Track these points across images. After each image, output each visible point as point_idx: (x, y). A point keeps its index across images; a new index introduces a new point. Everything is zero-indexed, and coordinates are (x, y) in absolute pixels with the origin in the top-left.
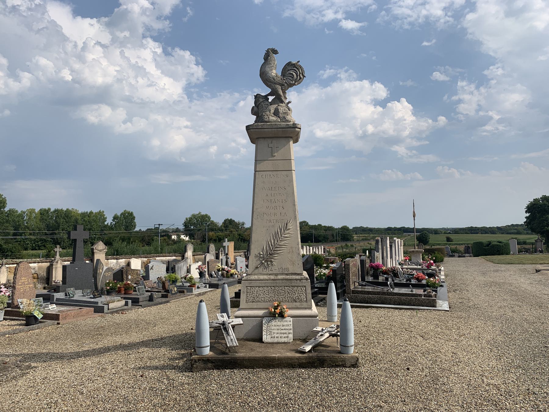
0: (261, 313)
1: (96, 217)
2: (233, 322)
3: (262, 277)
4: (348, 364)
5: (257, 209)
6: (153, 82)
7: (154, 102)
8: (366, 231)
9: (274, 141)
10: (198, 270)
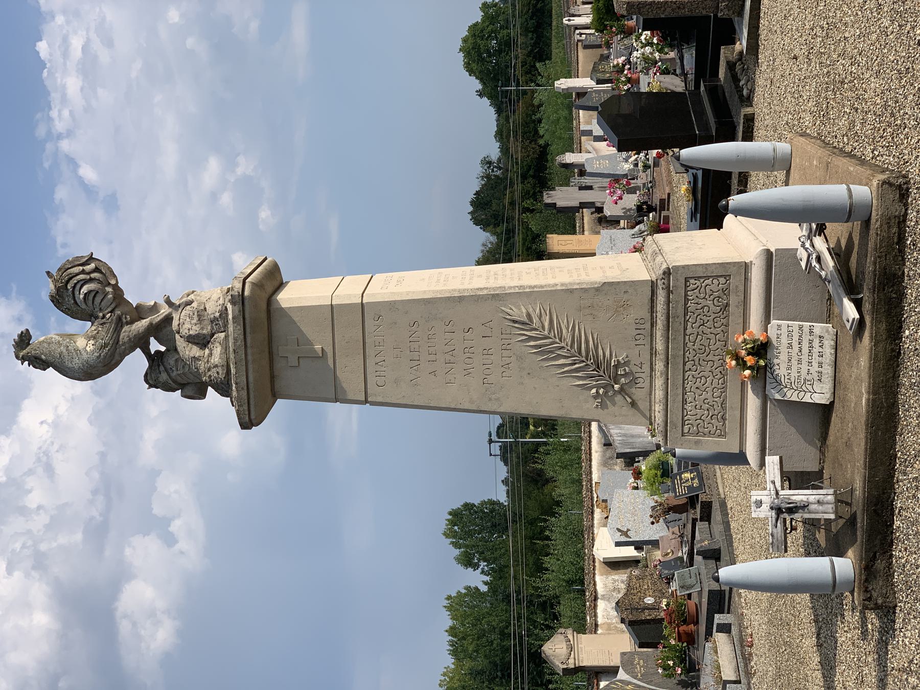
0: (753, 402)
1: (465, 616)
2: (773, 482)
3: (659, 394)
4: (898, 209)
5: (471, 402)
6: (39, 460)
7: (103, 455)
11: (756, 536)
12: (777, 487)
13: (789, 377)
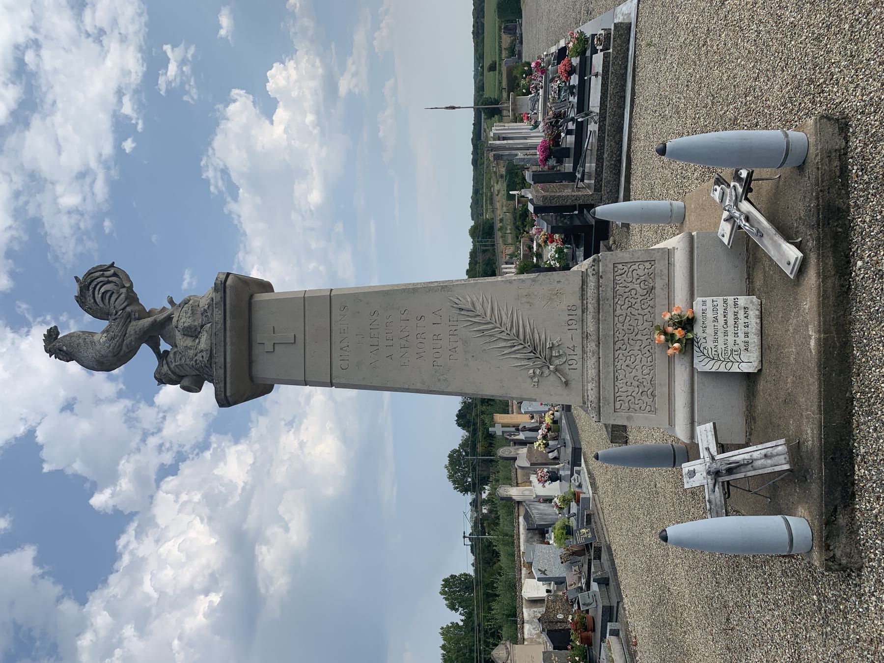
2: (708, 449)
3: (592, 373)
4: (840, 143)
8: (477, 200)
9: (258, 337)
10: (547, 484)
11: (638, 563)
12: (712, 453)
13: (716, 349)
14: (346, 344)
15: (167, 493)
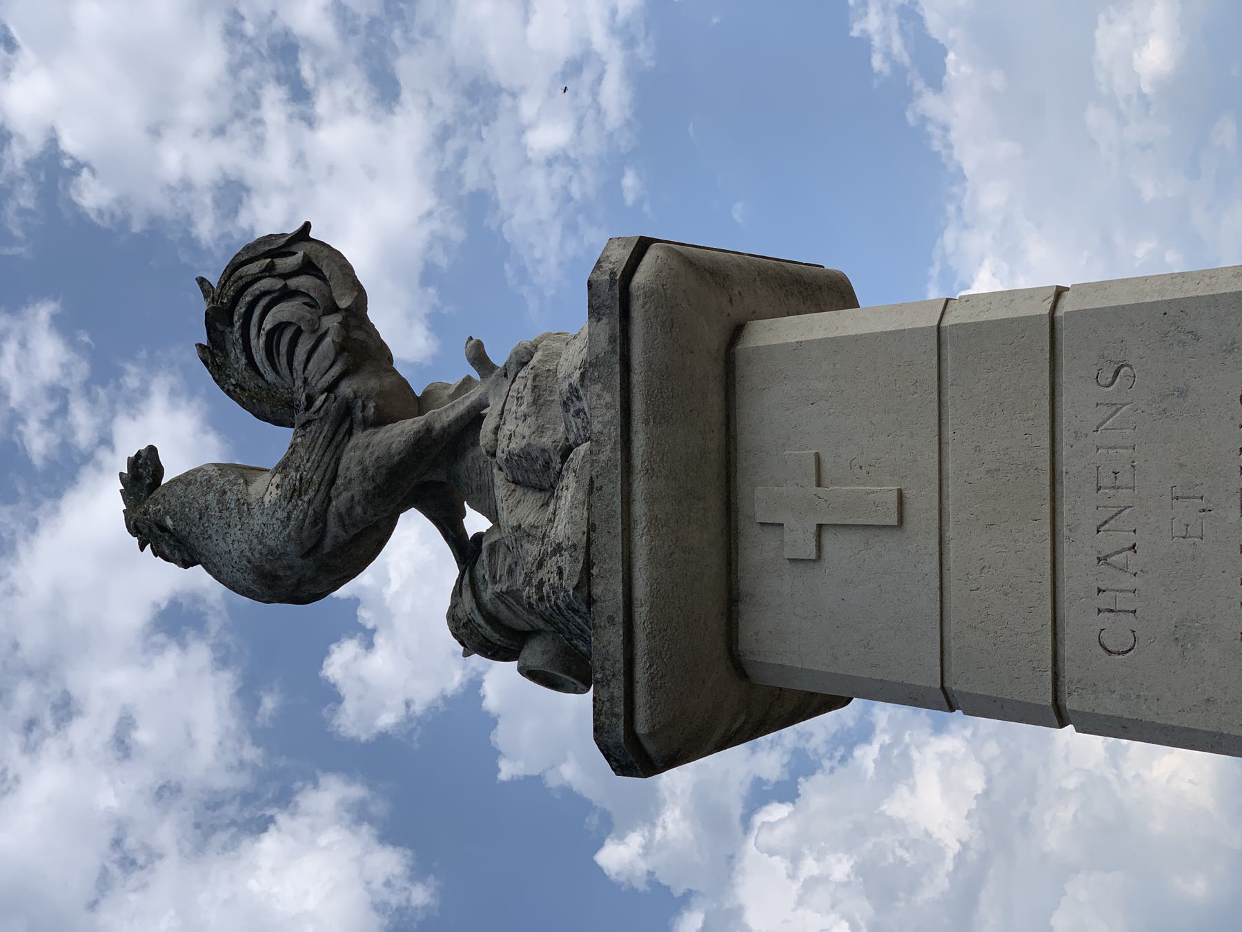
14: (1126, 539)
15: (771, 852)
